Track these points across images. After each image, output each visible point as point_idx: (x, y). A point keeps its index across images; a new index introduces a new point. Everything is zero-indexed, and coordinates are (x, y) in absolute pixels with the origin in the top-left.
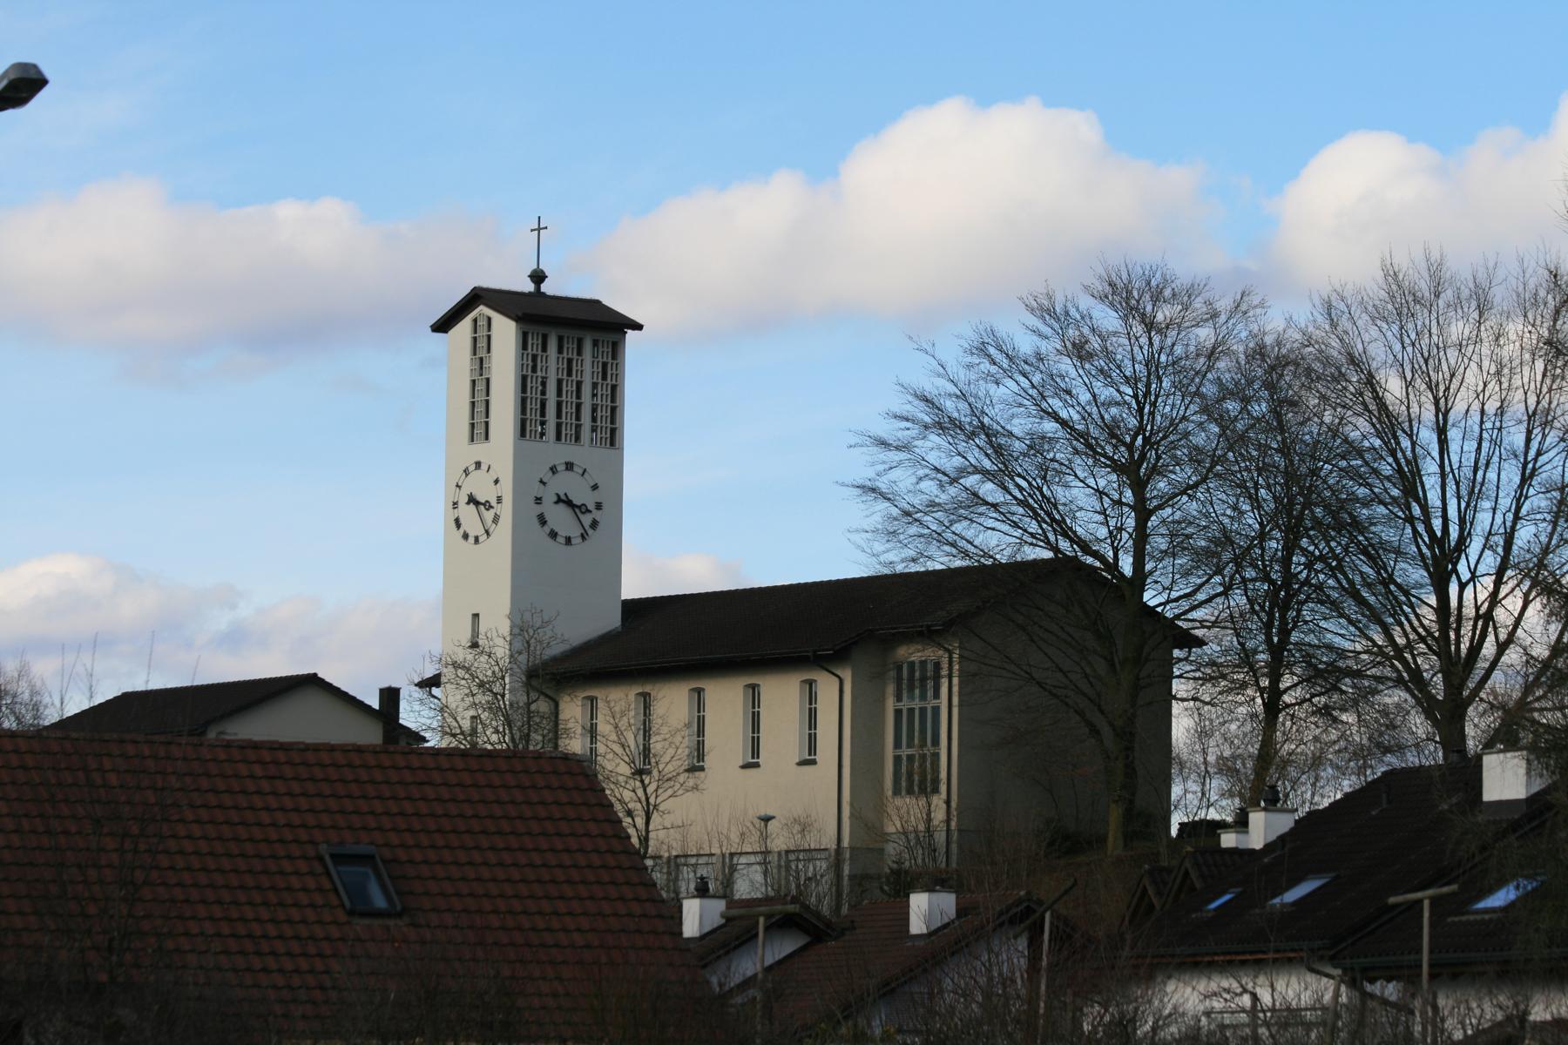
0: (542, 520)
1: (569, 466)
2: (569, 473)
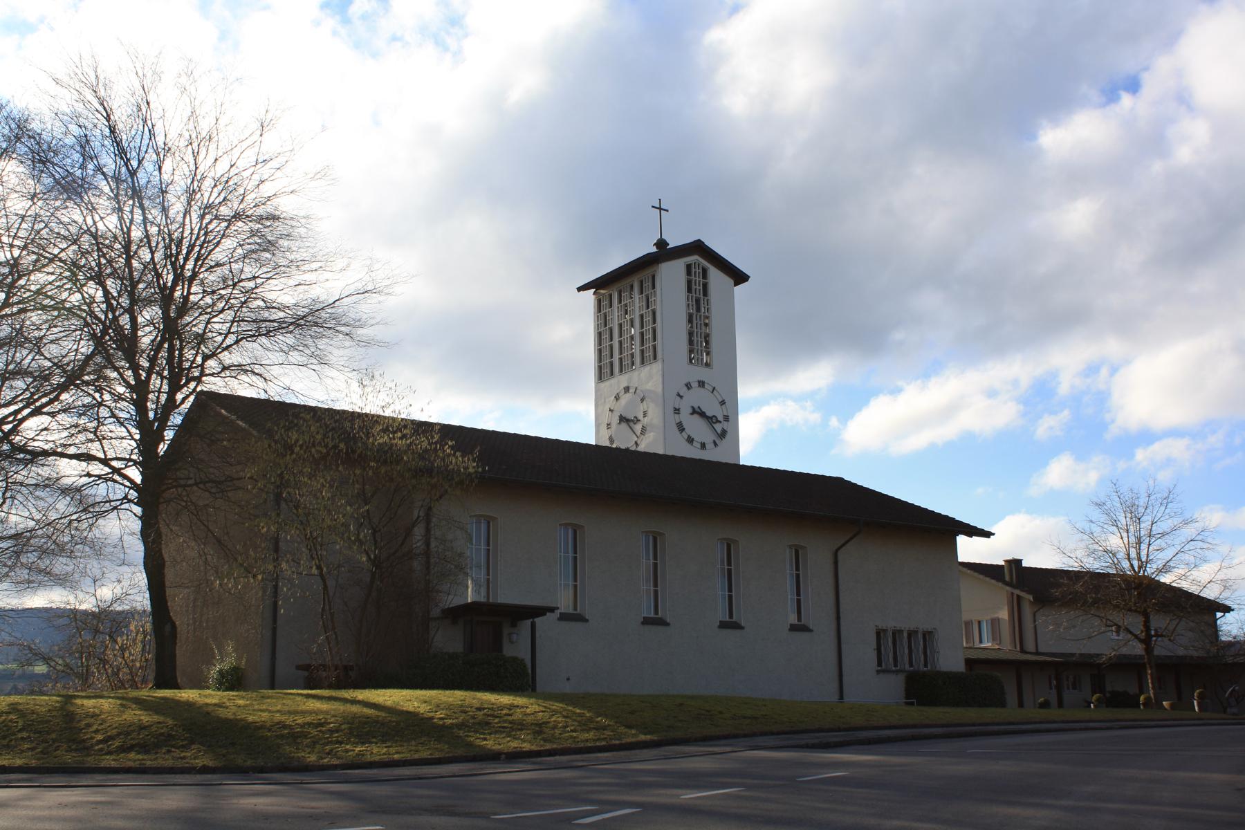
0: (681, 427)
1: (701, 384)
2: (702, 390)
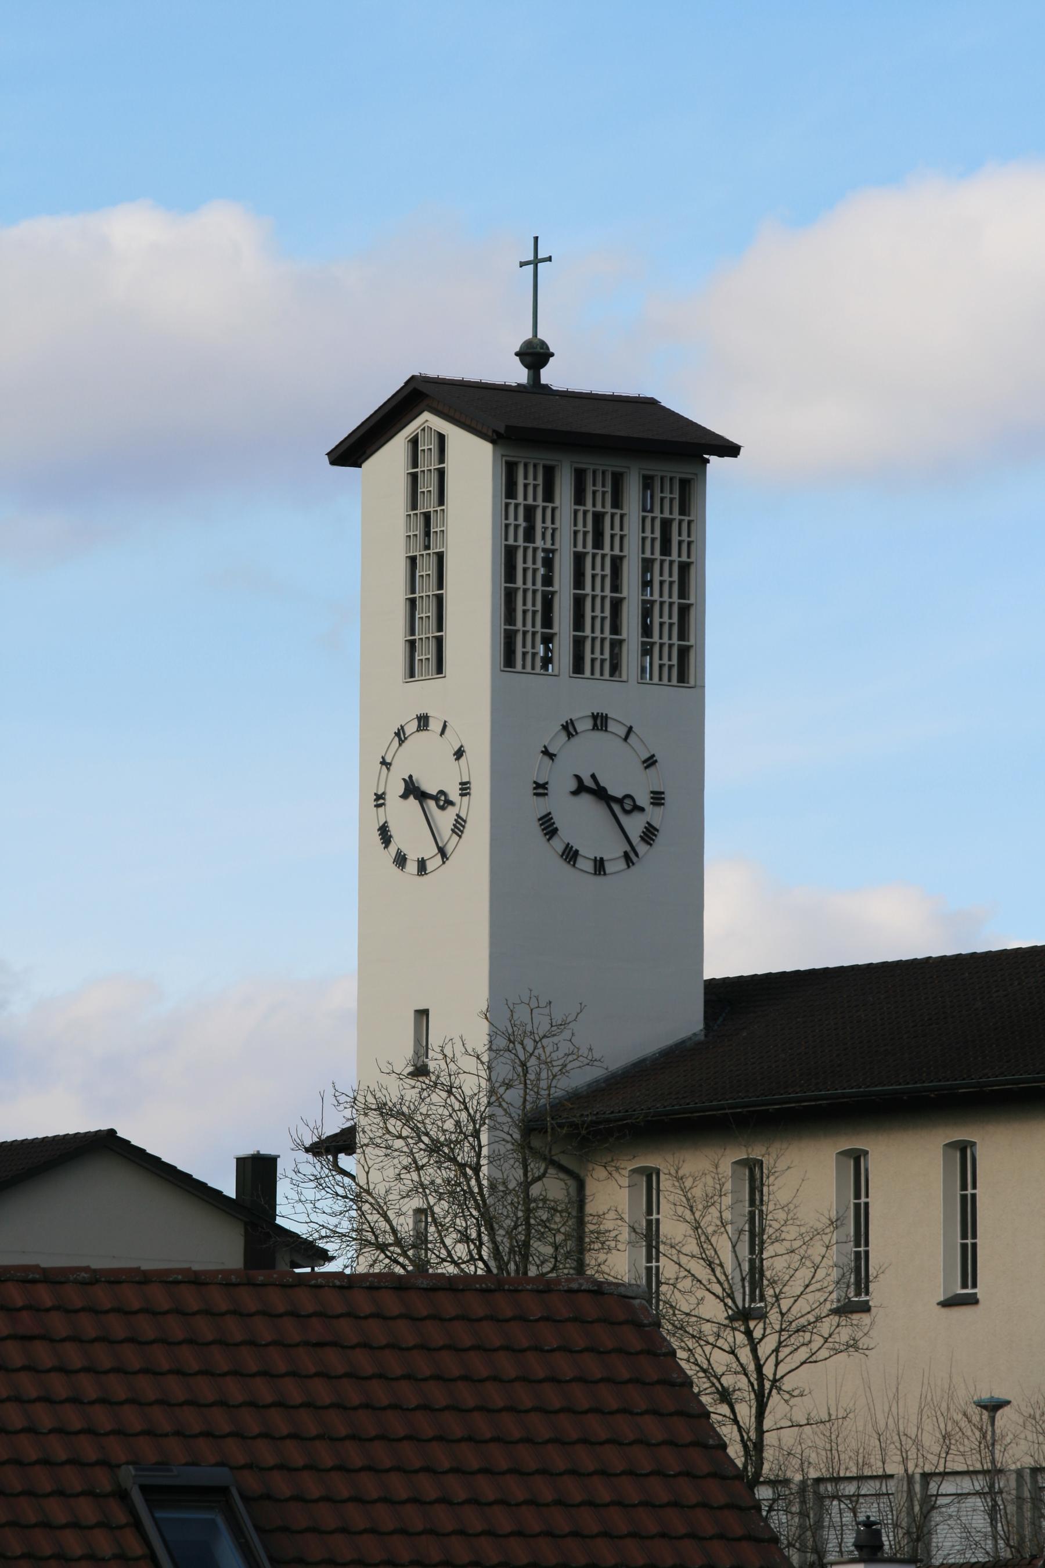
0: (549, 827)
1: (600, 722)
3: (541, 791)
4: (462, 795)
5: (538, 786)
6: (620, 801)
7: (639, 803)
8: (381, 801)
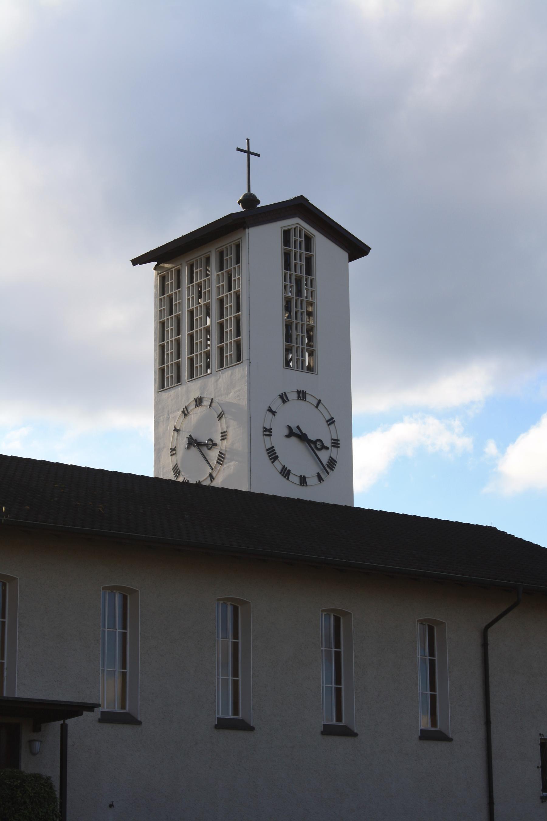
0: (272, 455)
1: (302, 395)
3: (267, 433)
4: (222, 440)
5: (266, 430)
6: (315, 443)
7: (325, 444)
8: (174, 452)
